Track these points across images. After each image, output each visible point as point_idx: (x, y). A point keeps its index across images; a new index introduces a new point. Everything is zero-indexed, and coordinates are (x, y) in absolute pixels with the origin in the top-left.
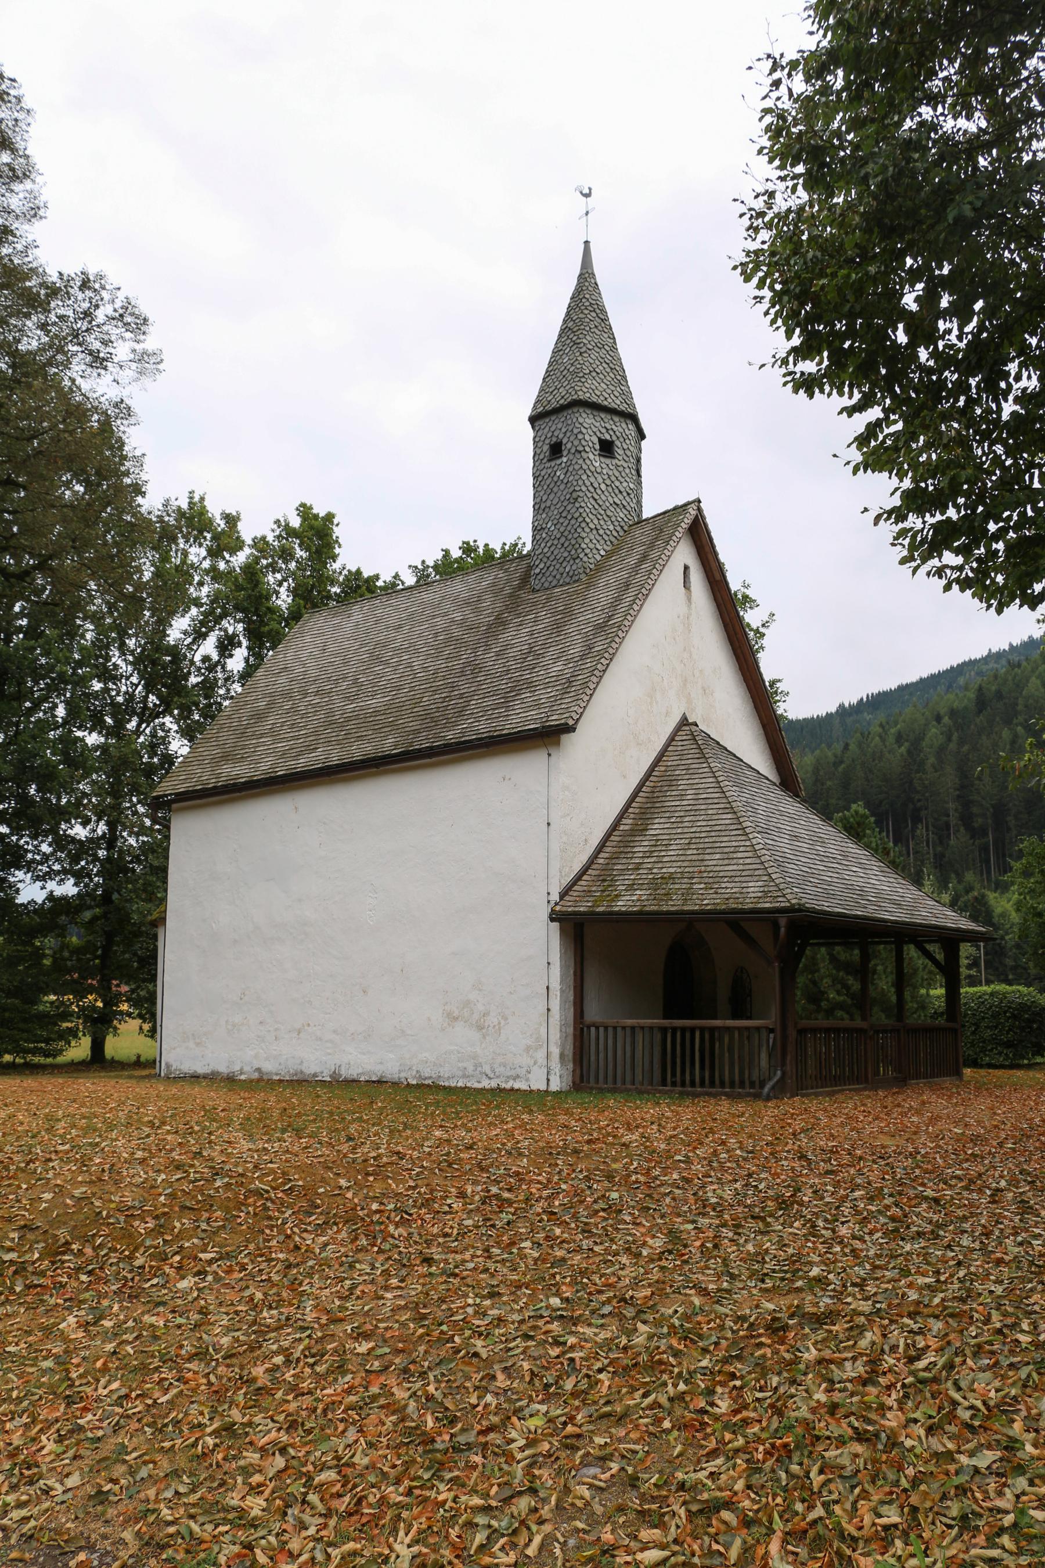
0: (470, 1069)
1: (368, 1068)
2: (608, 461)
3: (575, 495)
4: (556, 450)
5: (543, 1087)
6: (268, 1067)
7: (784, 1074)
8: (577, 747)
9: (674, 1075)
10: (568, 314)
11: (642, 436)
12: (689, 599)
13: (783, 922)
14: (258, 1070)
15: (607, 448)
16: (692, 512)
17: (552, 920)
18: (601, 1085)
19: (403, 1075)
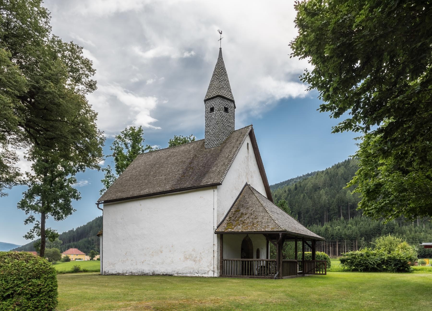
0: (192, 272)
1: (163, 271)
2: (227, 113)
3: (218, 122)
4: (212, 110)
5: (213, 276)
6: (134, 271)
7: (279, 272)
8: (222, 188)
9: (245, 272)
10: (215, 70)
11: (235, 107)
12: (248, 153)
13: (280, 234)
14: (131, 272)
15: (226, 110)
16: (250, 128)
17: (215, 233)
18: (228, 275)
19: (173, 273)
